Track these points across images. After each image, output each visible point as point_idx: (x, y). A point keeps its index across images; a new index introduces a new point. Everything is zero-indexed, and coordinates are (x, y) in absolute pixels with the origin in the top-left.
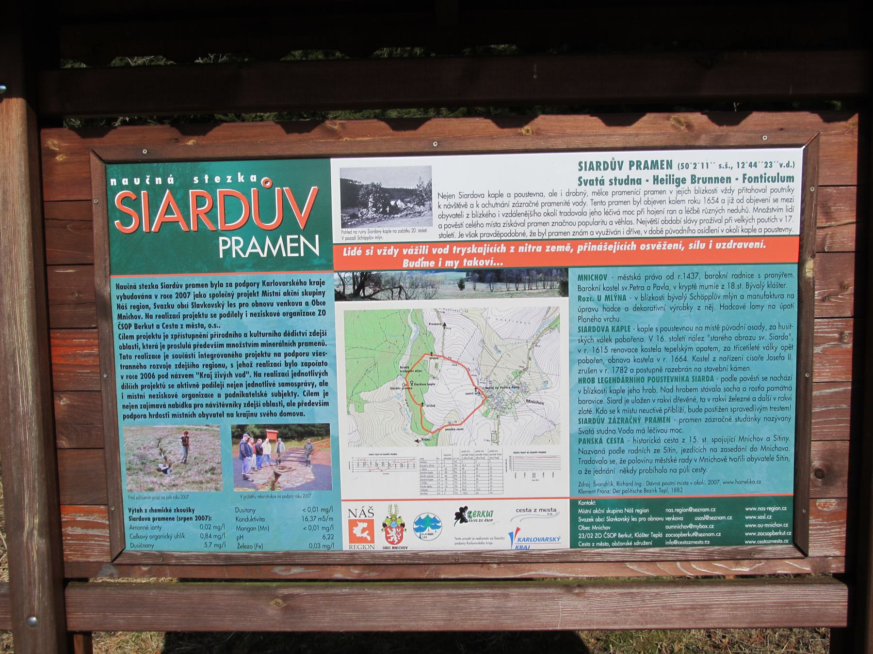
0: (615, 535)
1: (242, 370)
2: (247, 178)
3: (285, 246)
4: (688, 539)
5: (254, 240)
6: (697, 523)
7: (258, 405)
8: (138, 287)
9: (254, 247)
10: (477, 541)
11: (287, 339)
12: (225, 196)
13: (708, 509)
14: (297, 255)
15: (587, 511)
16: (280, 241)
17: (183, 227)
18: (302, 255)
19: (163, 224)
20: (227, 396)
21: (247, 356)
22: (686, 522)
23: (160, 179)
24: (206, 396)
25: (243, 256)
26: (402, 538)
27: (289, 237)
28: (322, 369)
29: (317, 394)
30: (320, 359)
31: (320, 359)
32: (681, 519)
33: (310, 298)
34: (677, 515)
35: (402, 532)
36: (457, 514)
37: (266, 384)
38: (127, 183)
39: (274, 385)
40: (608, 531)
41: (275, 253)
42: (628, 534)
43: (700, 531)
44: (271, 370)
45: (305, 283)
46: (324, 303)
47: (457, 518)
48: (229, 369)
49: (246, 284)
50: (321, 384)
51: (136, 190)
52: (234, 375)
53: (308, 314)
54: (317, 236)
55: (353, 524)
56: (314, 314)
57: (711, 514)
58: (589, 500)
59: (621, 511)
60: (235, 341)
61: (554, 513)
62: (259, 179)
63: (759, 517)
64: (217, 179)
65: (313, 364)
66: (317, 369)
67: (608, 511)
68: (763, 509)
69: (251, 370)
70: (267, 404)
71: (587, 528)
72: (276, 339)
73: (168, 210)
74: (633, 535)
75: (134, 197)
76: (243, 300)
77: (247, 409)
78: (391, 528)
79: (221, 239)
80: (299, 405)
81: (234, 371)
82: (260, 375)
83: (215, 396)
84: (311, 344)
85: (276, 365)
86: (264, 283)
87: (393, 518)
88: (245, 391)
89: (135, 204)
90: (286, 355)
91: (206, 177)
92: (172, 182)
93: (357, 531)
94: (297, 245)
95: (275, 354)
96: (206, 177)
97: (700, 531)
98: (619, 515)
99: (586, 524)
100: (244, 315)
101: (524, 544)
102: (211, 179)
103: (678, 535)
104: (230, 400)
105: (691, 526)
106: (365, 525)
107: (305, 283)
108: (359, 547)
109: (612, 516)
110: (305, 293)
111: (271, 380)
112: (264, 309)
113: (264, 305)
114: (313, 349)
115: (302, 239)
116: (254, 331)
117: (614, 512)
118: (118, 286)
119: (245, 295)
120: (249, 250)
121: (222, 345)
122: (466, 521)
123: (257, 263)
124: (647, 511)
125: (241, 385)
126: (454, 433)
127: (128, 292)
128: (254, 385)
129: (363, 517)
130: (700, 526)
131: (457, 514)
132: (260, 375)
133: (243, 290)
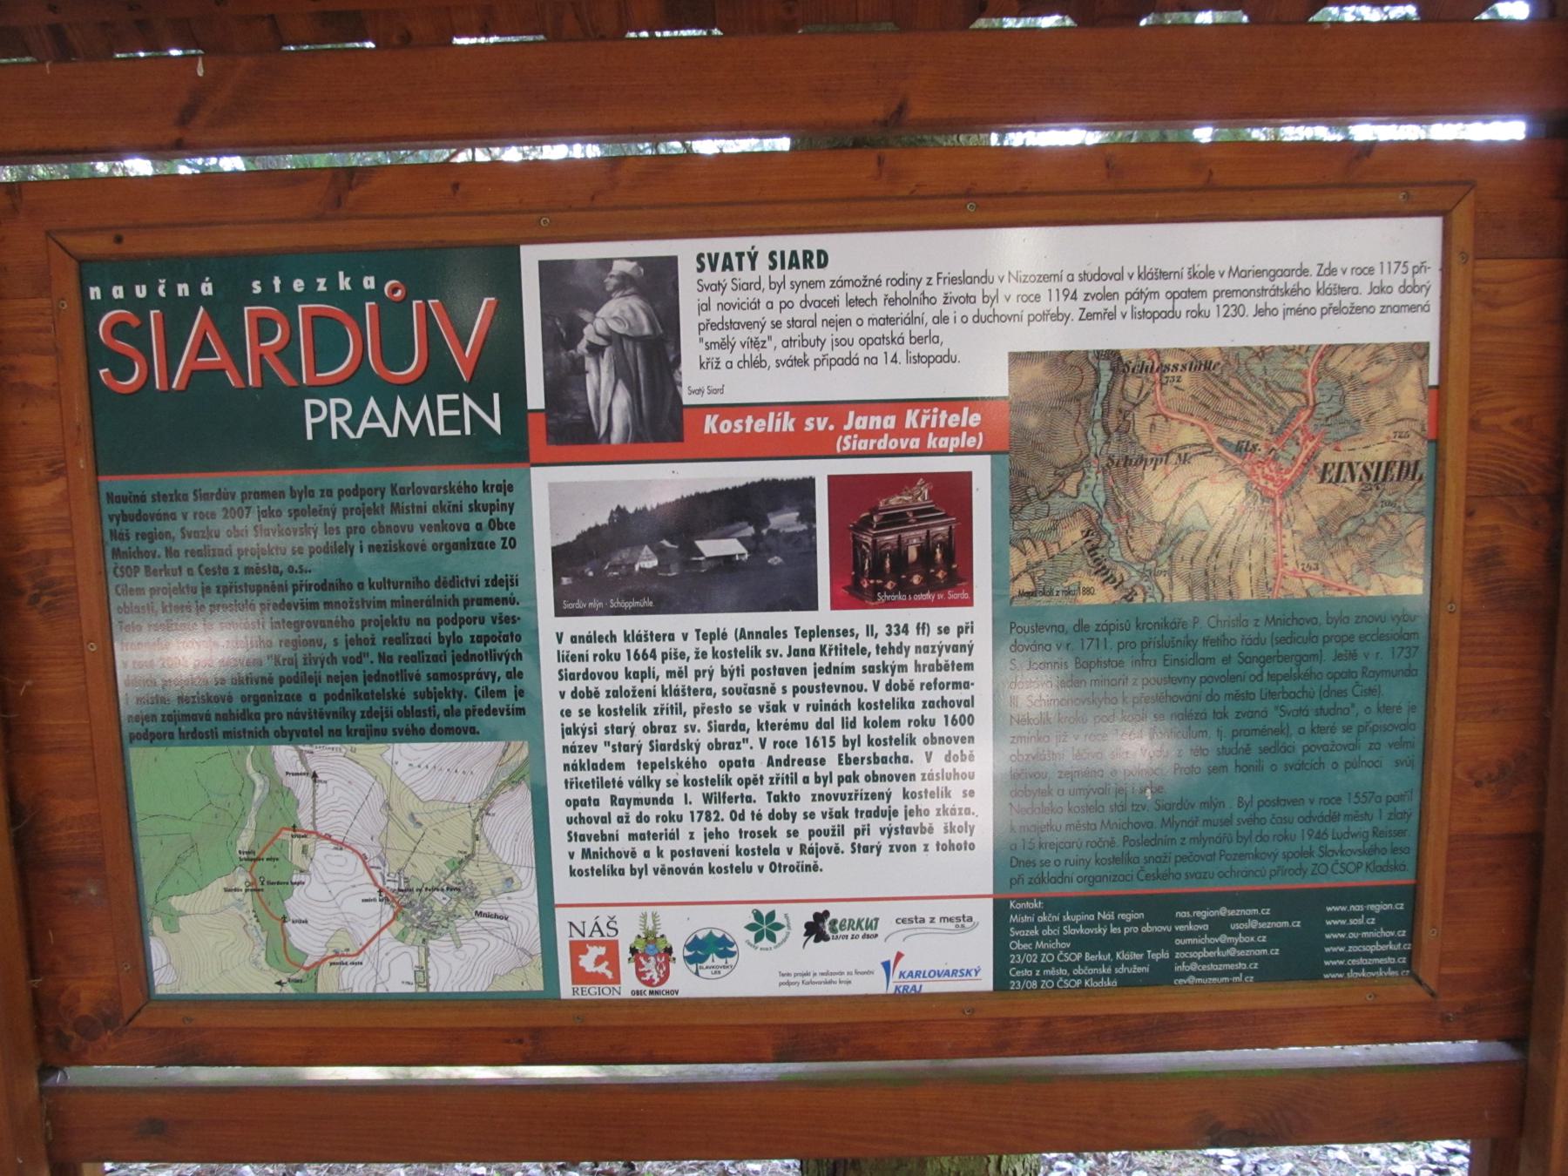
0: (1078, 956)
1: (354, 651)
2: (356, 283)
3: (434, 417)
4: (1217, 960)
5: (372, 404)
6: (1235, 933)
7: (389, 714)
8: (149, 499)
9: (373, 418)
10: (823, 978)
11: (440, 593)
12: (315, 319)
13: (1255, 911)
14: (458, 433)
15: (1026, 918)
16: (425, 406)
17: (232, 379)
18: (468, 432)
19: (194, 375)
20: (327, 698)
21: (365, 623)
22: (1213, 933)
23: (186, 286)
24: (288, 698)
25: (351, 436)
26: (667, 974)
27: (440, 398)
28: (511, 647)
29: (502, 693)
30: (506, 629)
31: (506, 629)
32: (1206, 927)
33: (484, 517)
34: (1197, 921)
35: (667, 963)
36: (808, 925)
37: (401, 676)
38: (121, 296)
39: (418, 677)
40: (1066, 950)
41: (414, 429)
42: (1104, 953)
43: (1241, 946)
44: (411, 650)
45: (474, 489)
46: (512, 526)
47: (808, 934)
48: (331, 648)
49: (358, 492)
50: (509, 675)
51: (140, 308)
52: (340, 660)
53: (481, 546)
54: (496, 396)
55: (578, 949)
56: (493, 545)
57: (1261, 919)
58: (1031, 900)
59: (1091, 917)
60: (341, 596)
61: (968, 924)
62: (380, 285)
63: (1352, 922)
64: (298, 285)
65: (495, 639)
66: (501, 647)
67: (1067, 918)
68: (1360, 908)
69: (373, 652)
70: (405, 713)
71: (1026, 946)
72: (421, 594)
73: (204, 348)
74: (1113, 956)
75: (135, 322)
76: (355, 520)
77: (367, 721)
78: (646, 957)
79: (308, 403)
80: (469, 713)
81: (340, 652)
82: (390, 660)
83: (306, 697)
84: (488, 601)
85: (420, 640)
86: (393, 488)
87: (650, 937)
88: (363, 689)
89: (139, 337)
90: (440, 622)
91: (277, 282)
92: (210, 292)
93: (587, 962)
94: (457, 413)
95: (420, 622)
96: (277, 282)
97: (1241, 946)
98: (1087, 924)
99: (1024, 940)
100: (357, 550)
101: (910, 983)
102: (287, 285)
103: (1199, 955)
104: (335, 706)
105: (1223, 939)
106: (602, 951)
107: (474, 489)
108: (592, 992)
109: (1074, 925)
110: (475, 507)
111: (412, 668)
112: (394, 538)
113: (397, 529)
114: (495, 610)
115: (468, 402)
116: (377, 579)
117: (1077, 918)
118: (110, 497)
119: (359, 511)
120: (365, 424)
121: (314, 606)
122: (826, 939)
123: (376, 449)
124: (1140, 915)
125: (355, 678)
126: (347, 970)
127: (131, 508)
128: (379, 677)
129: (597, 936)
130: (1241, 939)
131: (808, 925)
132: (390, 660)
133: (354, 502)
